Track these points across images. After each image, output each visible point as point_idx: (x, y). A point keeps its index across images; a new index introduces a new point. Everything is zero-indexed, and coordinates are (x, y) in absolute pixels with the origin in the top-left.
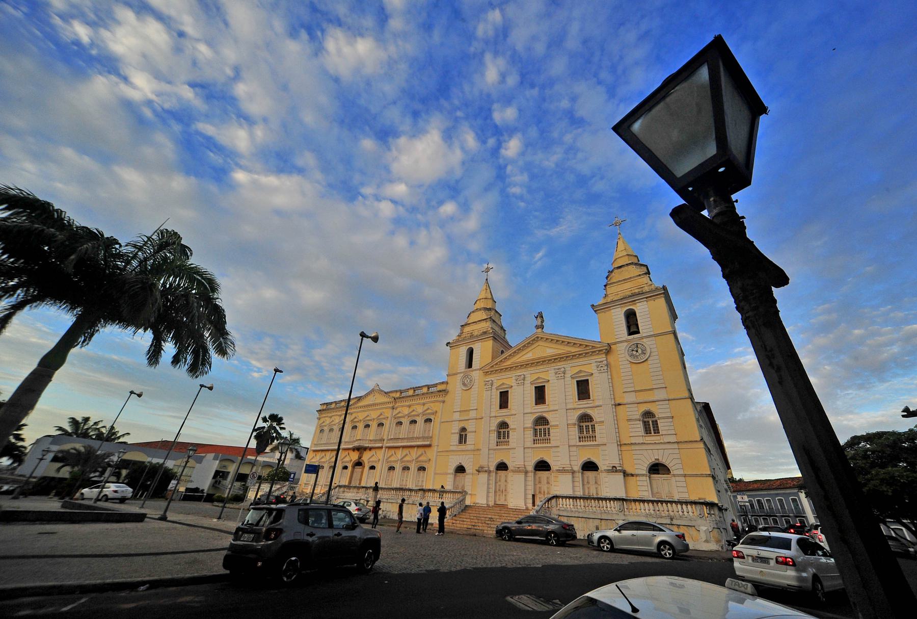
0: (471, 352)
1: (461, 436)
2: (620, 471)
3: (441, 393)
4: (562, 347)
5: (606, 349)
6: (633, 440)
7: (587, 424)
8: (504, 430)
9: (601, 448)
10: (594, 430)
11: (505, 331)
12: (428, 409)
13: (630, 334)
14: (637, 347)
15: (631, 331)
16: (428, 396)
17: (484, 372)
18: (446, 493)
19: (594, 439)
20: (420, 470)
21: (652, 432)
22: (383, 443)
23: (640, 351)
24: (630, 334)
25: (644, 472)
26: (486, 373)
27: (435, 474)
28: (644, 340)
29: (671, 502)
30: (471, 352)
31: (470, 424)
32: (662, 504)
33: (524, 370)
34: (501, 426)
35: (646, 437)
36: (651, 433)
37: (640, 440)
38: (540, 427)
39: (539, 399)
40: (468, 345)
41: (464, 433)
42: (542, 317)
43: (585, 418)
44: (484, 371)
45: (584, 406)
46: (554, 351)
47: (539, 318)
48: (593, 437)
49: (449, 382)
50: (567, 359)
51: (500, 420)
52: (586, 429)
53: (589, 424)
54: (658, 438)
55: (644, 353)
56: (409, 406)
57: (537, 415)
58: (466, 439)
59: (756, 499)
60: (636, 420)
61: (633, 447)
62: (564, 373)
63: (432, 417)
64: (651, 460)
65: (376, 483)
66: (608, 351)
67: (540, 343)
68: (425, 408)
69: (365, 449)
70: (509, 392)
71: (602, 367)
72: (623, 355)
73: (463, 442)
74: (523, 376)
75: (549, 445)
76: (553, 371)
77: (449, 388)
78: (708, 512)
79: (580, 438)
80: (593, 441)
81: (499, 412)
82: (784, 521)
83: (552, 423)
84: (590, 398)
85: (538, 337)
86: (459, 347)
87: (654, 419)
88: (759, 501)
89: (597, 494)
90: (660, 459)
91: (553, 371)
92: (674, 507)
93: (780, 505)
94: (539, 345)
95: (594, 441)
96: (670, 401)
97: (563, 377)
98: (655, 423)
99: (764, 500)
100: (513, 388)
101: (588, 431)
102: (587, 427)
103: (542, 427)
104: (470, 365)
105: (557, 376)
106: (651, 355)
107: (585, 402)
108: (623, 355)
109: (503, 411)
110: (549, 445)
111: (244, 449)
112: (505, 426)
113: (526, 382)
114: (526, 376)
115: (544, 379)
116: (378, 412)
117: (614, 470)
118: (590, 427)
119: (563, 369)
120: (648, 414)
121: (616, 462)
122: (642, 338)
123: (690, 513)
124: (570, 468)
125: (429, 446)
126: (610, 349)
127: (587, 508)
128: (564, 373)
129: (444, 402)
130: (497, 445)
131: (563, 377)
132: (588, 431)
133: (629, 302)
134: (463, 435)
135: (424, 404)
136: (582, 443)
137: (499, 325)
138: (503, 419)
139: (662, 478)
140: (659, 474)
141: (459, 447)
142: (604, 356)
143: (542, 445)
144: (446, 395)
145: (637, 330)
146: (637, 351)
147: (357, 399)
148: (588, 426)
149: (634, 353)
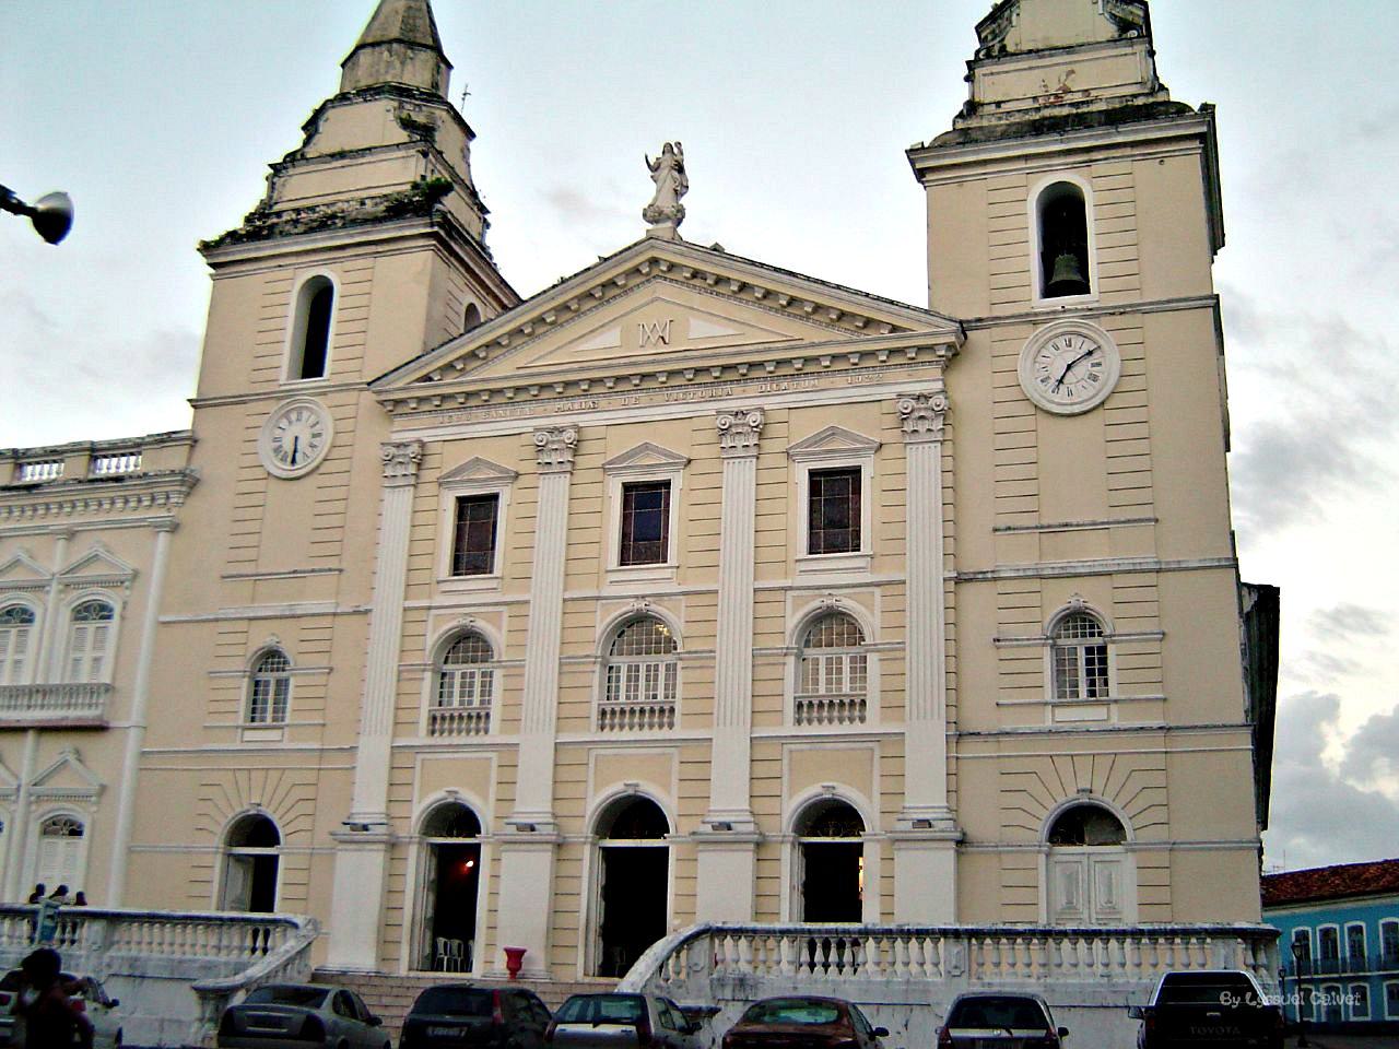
0: (319, 298)
4: (747, 312)
5: (950, 346)
11: (483, 210)
12: (95, 558)
13: (1050, 290)
15: (1057, 278)
17: (382, 403)
19: (482, 725)
20: (55, 833)
24: (1050, 290)
26: (394, 407)
29: (1106, 935)
30: (319, 298)
32: (878, 942)
33: (426, 419)
35: (1057, 710)
37: (1047, 720)
39: (831, 524)
41: (270, 677)
42: (680, 169)
44: (383, 397)
46: (718, 330)
47: (664, 173)
48: (479, 717)
49: (200, 435)
50: (446, 406)
56: (71, 535)
59: (1318, 929)
60: (1029, 642)
62: (575, 453)
63: (113, 599)
64: (1066, 796)
66: (955, 355)
67: (662, 289)
68: (82, 549)
70: (502, 503)
73: (269, 715)
74: (415, 448)
75: (857, 728)
77: (202, 463)
78: (1251, 961)
79: (604, 713)
80: (631, 728)
82: (1385, 990)
84: (857, 548)
85: (654, 261)
88: (1327, 935)
94: (657, 299)
95: (666, 728)
96: (337, 618)
97: (754, 452)
98: (1097, 661)
99: (1342, 928)
104: (312, 362)
105: (389, 472)
106: (322, 470)
112: (475, 650)
113: (582, 461)
114: (432, 449)
119: (415, 448)
120: (271, 657)
123: (928, 967)
124: (751, 827)
125: (99, 729)
128: (575, 453)
129: (174, 528)
130: (433, 732)
131: (754, 452)
133: (1133, 144)
134: (267, 683)
135: (71, 535)
137: (468, 188)
138: (465, 621)
139: (1093, 858)
140: (1081, 842)
141: (249, 735)
142: (936, 372)
143: (636, 734)
144: (188, 495)
145: (1077, 277)
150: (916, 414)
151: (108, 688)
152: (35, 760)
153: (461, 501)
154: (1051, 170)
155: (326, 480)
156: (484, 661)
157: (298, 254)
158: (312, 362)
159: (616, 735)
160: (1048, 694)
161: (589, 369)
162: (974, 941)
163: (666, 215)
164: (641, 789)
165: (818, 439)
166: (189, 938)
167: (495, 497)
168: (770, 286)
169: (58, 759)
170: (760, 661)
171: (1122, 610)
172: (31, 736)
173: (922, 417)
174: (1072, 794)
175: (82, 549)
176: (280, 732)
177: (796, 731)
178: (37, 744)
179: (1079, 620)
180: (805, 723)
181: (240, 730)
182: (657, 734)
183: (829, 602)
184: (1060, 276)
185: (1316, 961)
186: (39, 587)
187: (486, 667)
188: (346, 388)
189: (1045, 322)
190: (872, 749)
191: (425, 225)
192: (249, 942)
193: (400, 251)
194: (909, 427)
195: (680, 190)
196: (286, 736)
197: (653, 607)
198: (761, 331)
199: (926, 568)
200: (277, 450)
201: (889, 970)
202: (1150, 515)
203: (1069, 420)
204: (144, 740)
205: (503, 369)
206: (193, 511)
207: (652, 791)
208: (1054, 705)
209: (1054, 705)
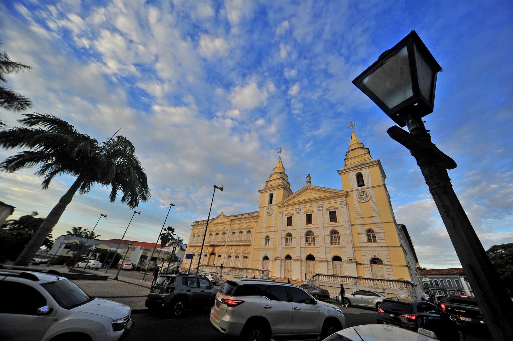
0: (271, 196)
1: (266, 240)
2: (354, 262)
3: (256, 217)
5: (346, 195)
6: (361, 245)
7: (312, 236)
8: (289, 238)
9: (343, 249)
10: (339, 239)
11: (290, 184)
13: (359, 186)
14: (363, 193)
15: (360, 184)
16: (249, 219)
19: (339, 243)
22: (225, 243)
23: (365, 196)
24: (359, 186)
25: (368, 263)
26: (280, 207)
27: (253, 260)
28: (367, 190)
30: (271, 196)
31: (271, 234)
34: (288, 235)
37: (365, 245)
38: (309, 236)
41: (268, 239)
43: (334, 232)
45: (333, 226)
51: (287, 232)
55: (367, 197)
58: (269, 242)
61: (362, 249)
62: (322, 208)
65: (222, 264)
67: (309, 191)
68: (248, 224)
69: (216, 246)
72: (355, 198)
75: (314, 246)
76: (316, 206)
77: (260, 214)
85: (308, 188)
86: (265, 193)
91: (295, 210)
97: (322, 210)
98: (374, 236)
100: (339, 209)
101: (336, 239)
103: (310, 237)
104: (271, 202)
107: (334, 223)
108: (355, 198)
110: (314, 246)
111: (155, 245)
114: (302, 209)
116: (223, 227)
117: (350, 261)
118: (337, 237)
119: (322, 205)
121: (352, 257)
122: (366, 188)
124: (326, 259)
125: (250, 245)
126: (348, 195)
128: (322, 208)
132: (336, 239)
134: (267, 240)
135: (247, 223)
136: (332, 246)
137: (287, 181)
143: (310, 246)
144: (258, 218)
146: (363, 196)
147: (212, 220)
148: (336, 236)
149: (362, 196)
150: (343, 203)
151: (251, 241)
152: (235, 249)
153: (287, 217)
155: (371, 202)
156: (313, 235)
157: (279, 188)
158: (271, 202)
159: (308, 246)
161: (313, 199)
167: (291, 217)
168: (319, 189)
169: (237, 249)
170: (325, 236)
171: (377, 229)
172: (198, 247)
173: (343, 204)
174: (373, 256)
175: (248, 224)
178: (235, 247)
182: (313, 246)
183: (289, 232)
185: (435, 286)
186: (236, 230)
187: (338, 235)
188: (275, 205)
192: (262, 273)
195: (310, 179)
197: (336, 228)
198: (321, 195)
201: (329, 281)
202: (379, 215)
203: (366, 203)
204: (254, 247)
205: (292, 202)
206: (259, 220)
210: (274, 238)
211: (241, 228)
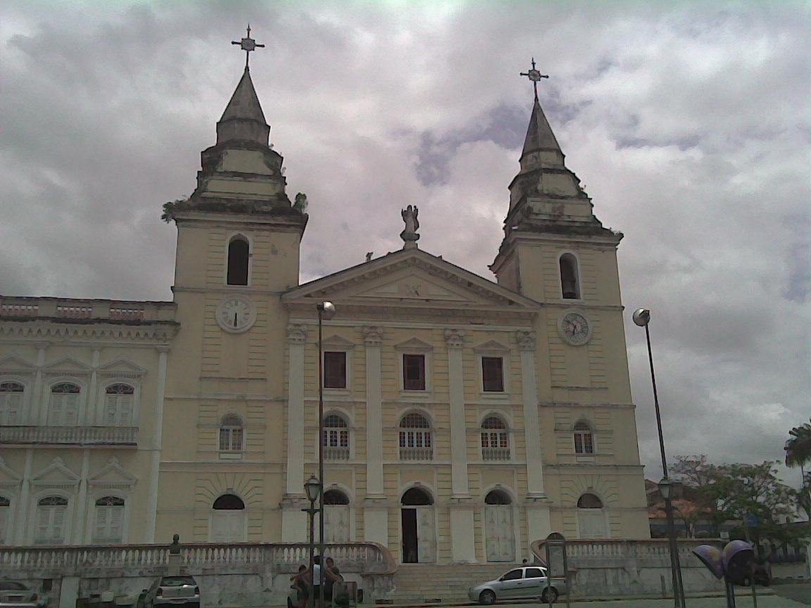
8: (334, 429)
13: (566, 296)
18: (195, 550)
21: (231, 446)
24: (566, 296)
35: (221, 455)
36: (228, 448)
38: (411, 430)
40: (236, 229)
43: (493, 422)
46: (445, 293)
51: (487, 412)
52: (336, 441)
53: (423, 431)
54: (239, 456)
57: (406, 409)
64: (221, 491)
71: (527, 341)
75: (507, 462)
80: (414, 459)
81: (403, 394)
83: (435, 426)
85: (414, 259)
87: (587, 432)
89: (349, 540)
90: (235, 490)
92: (154, 554)
93: (706, 541)
94: (413, 275)
101: (494, 444)
102: (494, 436)
103: (415, 430)
107: (418, 393)
109: (332, 393)
115: (422, 343)
120: (232, 420)
127: (662, 555)
129: (168, 352)
132: (494, 444)
133: (556, 241)
141: (223, 456)
154: (564, 247)
159: (490, 462)
160: (217, 448)
162: (595, 546)
163: (409, 236)
164: (422, 484)
165: (486, 345)
166: (252, 554)
173: (454, 339)
176: (240, 455)
177: (400, 462)
179: (232, 420)
180: (403, 459)
181: (218, 454)
184: (567, 290)
189: (566, 308)
190: (513, 471)
191: (286, 221)
193: (190, 226)
194: (521, 344)
196: (244, 457)
199: (531, 403)
200: (225, 319)
207: (425, 484)
208: (220, 453)
209: (220, 453)
210: (264, 453)
211: (123, 369)
